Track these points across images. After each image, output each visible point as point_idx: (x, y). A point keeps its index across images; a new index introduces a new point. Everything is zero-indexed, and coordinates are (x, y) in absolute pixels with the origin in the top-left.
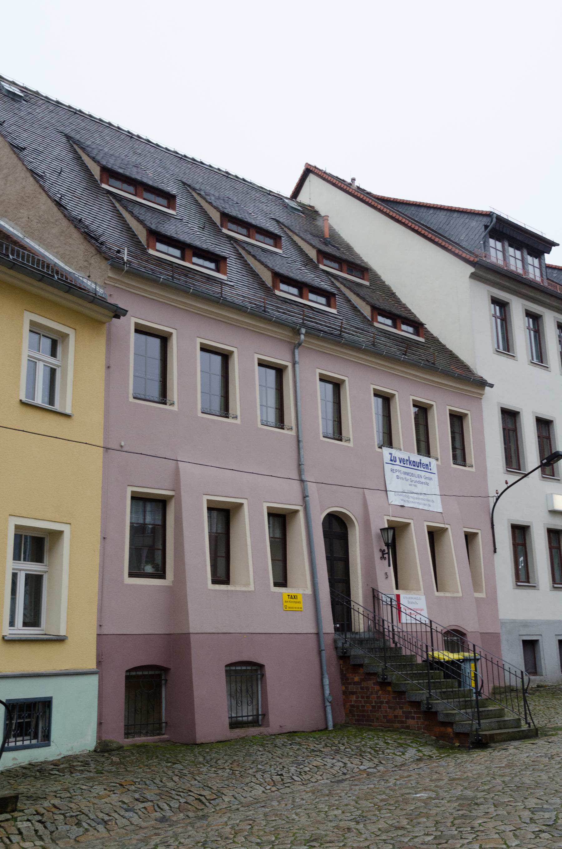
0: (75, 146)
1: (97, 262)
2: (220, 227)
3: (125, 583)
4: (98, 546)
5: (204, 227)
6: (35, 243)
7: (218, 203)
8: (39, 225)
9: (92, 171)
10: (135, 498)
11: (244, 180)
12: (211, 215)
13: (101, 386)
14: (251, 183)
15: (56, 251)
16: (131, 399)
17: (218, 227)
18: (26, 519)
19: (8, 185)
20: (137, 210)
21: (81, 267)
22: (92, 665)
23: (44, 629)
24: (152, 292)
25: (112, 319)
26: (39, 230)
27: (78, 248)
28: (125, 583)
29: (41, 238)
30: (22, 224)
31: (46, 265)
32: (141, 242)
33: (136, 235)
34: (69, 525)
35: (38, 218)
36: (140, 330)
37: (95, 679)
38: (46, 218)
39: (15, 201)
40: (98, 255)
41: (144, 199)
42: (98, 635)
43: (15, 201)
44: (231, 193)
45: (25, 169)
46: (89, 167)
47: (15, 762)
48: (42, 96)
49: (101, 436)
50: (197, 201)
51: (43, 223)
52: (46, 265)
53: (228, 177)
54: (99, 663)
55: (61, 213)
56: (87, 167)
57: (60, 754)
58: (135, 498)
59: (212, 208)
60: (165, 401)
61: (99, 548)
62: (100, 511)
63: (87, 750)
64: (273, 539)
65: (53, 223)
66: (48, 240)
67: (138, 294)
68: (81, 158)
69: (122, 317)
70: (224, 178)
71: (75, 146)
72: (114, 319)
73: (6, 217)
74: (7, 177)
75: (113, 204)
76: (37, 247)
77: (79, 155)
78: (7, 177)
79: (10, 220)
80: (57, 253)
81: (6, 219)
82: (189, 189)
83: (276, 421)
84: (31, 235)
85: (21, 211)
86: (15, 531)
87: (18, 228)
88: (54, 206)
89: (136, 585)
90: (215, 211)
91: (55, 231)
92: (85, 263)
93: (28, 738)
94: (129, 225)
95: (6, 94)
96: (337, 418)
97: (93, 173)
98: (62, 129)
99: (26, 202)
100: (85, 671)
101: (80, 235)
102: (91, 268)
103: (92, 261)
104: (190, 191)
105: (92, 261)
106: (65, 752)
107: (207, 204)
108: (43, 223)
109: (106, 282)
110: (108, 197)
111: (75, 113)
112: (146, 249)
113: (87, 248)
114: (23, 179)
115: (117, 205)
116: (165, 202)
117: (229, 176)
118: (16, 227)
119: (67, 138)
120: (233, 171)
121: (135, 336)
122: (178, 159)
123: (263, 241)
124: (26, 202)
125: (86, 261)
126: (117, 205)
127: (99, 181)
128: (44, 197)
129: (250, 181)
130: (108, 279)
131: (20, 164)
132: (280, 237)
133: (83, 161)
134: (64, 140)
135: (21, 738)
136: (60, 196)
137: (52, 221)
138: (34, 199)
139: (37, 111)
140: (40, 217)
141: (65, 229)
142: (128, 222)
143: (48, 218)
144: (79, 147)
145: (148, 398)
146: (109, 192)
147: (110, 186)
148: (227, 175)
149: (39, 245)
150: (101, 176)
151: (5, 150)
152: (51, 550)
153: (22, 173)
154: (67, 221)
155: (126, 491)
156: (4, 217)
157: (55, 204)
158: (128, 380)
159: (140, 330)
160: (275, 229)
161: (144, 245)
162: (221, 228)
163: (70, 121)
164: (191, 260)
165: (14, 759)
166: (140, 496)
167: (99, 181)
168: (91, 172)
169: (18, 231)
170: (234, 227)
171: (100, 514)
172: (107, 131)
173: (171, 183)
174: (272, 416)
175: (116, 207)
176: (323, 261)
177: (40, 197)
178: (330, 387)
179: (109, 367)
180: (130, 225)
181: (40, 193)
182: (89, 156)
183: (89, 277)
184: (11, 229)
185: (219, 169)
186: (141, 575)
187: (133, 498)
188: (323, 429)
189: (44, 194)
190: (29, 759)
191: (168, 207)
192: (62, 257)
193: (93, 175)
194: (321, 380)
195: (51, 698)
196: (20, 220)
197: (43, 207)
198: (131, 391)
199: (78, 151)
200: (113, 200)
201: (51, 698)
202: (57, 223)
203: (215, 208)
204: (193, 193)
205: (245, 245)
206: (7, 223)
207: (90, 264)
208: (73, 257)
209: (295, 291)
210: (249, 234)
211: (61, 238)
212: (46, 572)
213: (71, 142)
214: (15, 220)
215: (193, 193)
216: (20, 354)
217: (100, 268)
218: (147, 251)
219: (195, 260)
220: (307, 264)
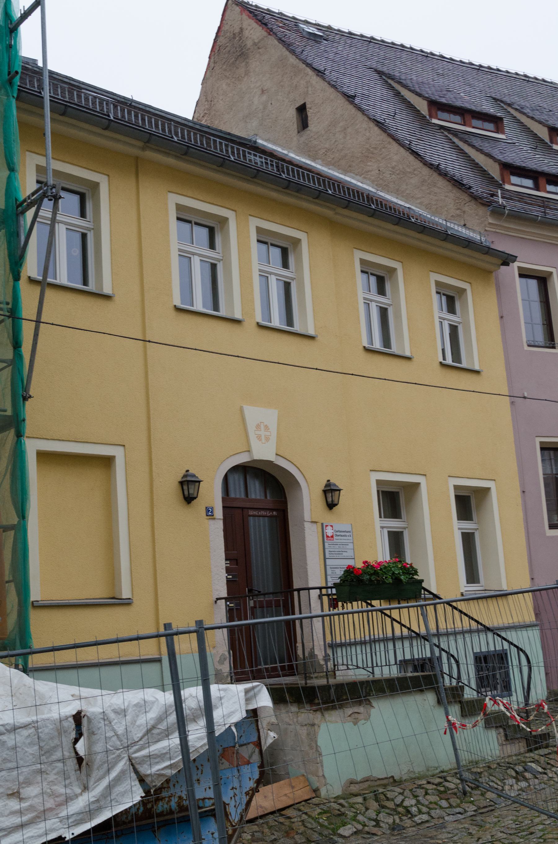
0: (390, 81)
1: (471, 208)
2: (549, 143)
5: (537, 147)
6: (392, 196)
7: (543, 117)
8: (393, 176)
9: (416, 106)
10: (545, 448)
11: (544, 80)
12: (535, 132)
13: (498, 337)
14: (551, 83)
15: (418, 201)
16: (526, 348)
17: (547, 143)
19: (348, 138)
20: (477, 142)
21: (452, 216)
23: (483, 585)
25: (499, 268)
26: (394, 182)
27: (446, 196)
29: (398, 190)
30: (373, 178)
32: (493, 178)
33: (485, 171)
34: (493, 482)
35: (390, 169)
36: (524, 274)
38: (401, 168)
39: (360, 155)
40: (473, 202)
41: (474, 127)
43: (360, 155)
44: (539, 100)
45: (366, 119)
46: (412, 103)
48: (335, 30)
49: (507, 388)
50: (515, 117)
51: (398, 174)
53: (528, 81)
54: (537, 615)
55: (419, 162)
56: (409, 102)
58: (545, 448)
59: (537, 124)
60: (553, 344)
61: (521, 502)
62: (516, 464)
64: (545, 476)
65: (410, 173)
66: (407, 192)
68: (400, 93)
69: (511, 264)
70: (525, 82)
71: (390, 81)
72: (502, 267)
73: (351, 172)
74: (345, 129)
75: (451, 139)
76: (395, 200)
77: (396, 90)
78: (345, 129)
79: (357, 175)
80: (421, 203)
81: (352, 174)
82: (502, 105)
83: (545, 340)
84: (386, 188)
85: (369, 164)
86: (455, 492)
87: (368, 182)
88: (410, 155)
90: (540, 126)
91: (414, 181)
92: (458, 212)
93: (488, 689)
94: (474, 161)
95: (308, 37)
96: (546, 320)
97: (418, 108)
98: (368, 63)
99: (373, 153)
101: (448, 183)
102: (465, 216)
103: (466, 209)
104: (505, 107)
105: (466, 209)
107: (529, 120)
108: (398, 174)
109: (487, 229)
110: (443, 133)
111: (370, 42)
112: (501, 185)
113: (458, 195)
114: (366, 130)
115: (455, 140)
116: (491, 126)
117: (530, 80)
118: (365, 181)
119: (379, 74)
120: (531, 74)
121: (520, 281)
122: (476, 71)
123: (481, 127)
124: (373, 153)
125: (458, 209)
126: (455, 140)
127: (428, 117)
128: (395, 146)
129: (550, 81)
130: (488, 226)
131: (359, 114)
132: (501, 119)
133: (402, 96)
134: (376, 76)
136: (409, 143)
137: (409, 170)
138: (383, 150)
139: (340, 49)
140: (393, 168)
141: (426, 178)
142: (472, 157)
143: (403, 168)
144: (395, 82)
145: (537, 344)
146: (442, 127)
147: (439, 120)
148: (527, 79)
149: (397, 198)
150: (429, 110)
151: (339, 101)
152: (478, 506)
153: (362, 123)
154: (428, 169)
155: (535, 442)
156: (348, 172)
157: (410, 153)
158: (521, 328)
159: (524, 274)
160: (489, 108)
161: (498, 180)
162: (551, 145)
163: (370, 52)
164: (510, 181)
166: (550, 446)
167: (428, 117)
168: (416, 108)
169: (369, 185)
170: (445, 115)
171: (516, 468)
172: (404, 55)
173: (485, 103)
174: (540, 336)
175: (454, 143)
176: (437, 115)
177: (389, 146)
178: (533, 284)
180: (477, 161)
181: (389, 143)
182: (410, 91)
183: (465, 225)
184: (359, 184)
185: (517, 74)
187: (542, 449)
188: (527, 337)
189: (394, 143)
191: (497, 132)
192: (428, 207)
193: (419, 111)
194: (521, 276)
196: (369, 173)
197: (396, 158)
198: (525, 340)
199: (395, 86)
200: (449, 136)
202: (415, 172)
203: (540, 122)
204: (509, 109)
205: (466, 137)
206: (353, 178)
207: (464, 212)
208: (441, 207)
209: (529, 183)
210: (464, 122)
211: (423, 188)
212: (476, 529)
213: (384, 77)
214: (363, 174)
215: (509, 109)
216: (433, 317)
217: (476, 215)
218: (503, 186)
219: (550, 188)
220: (537, 147)
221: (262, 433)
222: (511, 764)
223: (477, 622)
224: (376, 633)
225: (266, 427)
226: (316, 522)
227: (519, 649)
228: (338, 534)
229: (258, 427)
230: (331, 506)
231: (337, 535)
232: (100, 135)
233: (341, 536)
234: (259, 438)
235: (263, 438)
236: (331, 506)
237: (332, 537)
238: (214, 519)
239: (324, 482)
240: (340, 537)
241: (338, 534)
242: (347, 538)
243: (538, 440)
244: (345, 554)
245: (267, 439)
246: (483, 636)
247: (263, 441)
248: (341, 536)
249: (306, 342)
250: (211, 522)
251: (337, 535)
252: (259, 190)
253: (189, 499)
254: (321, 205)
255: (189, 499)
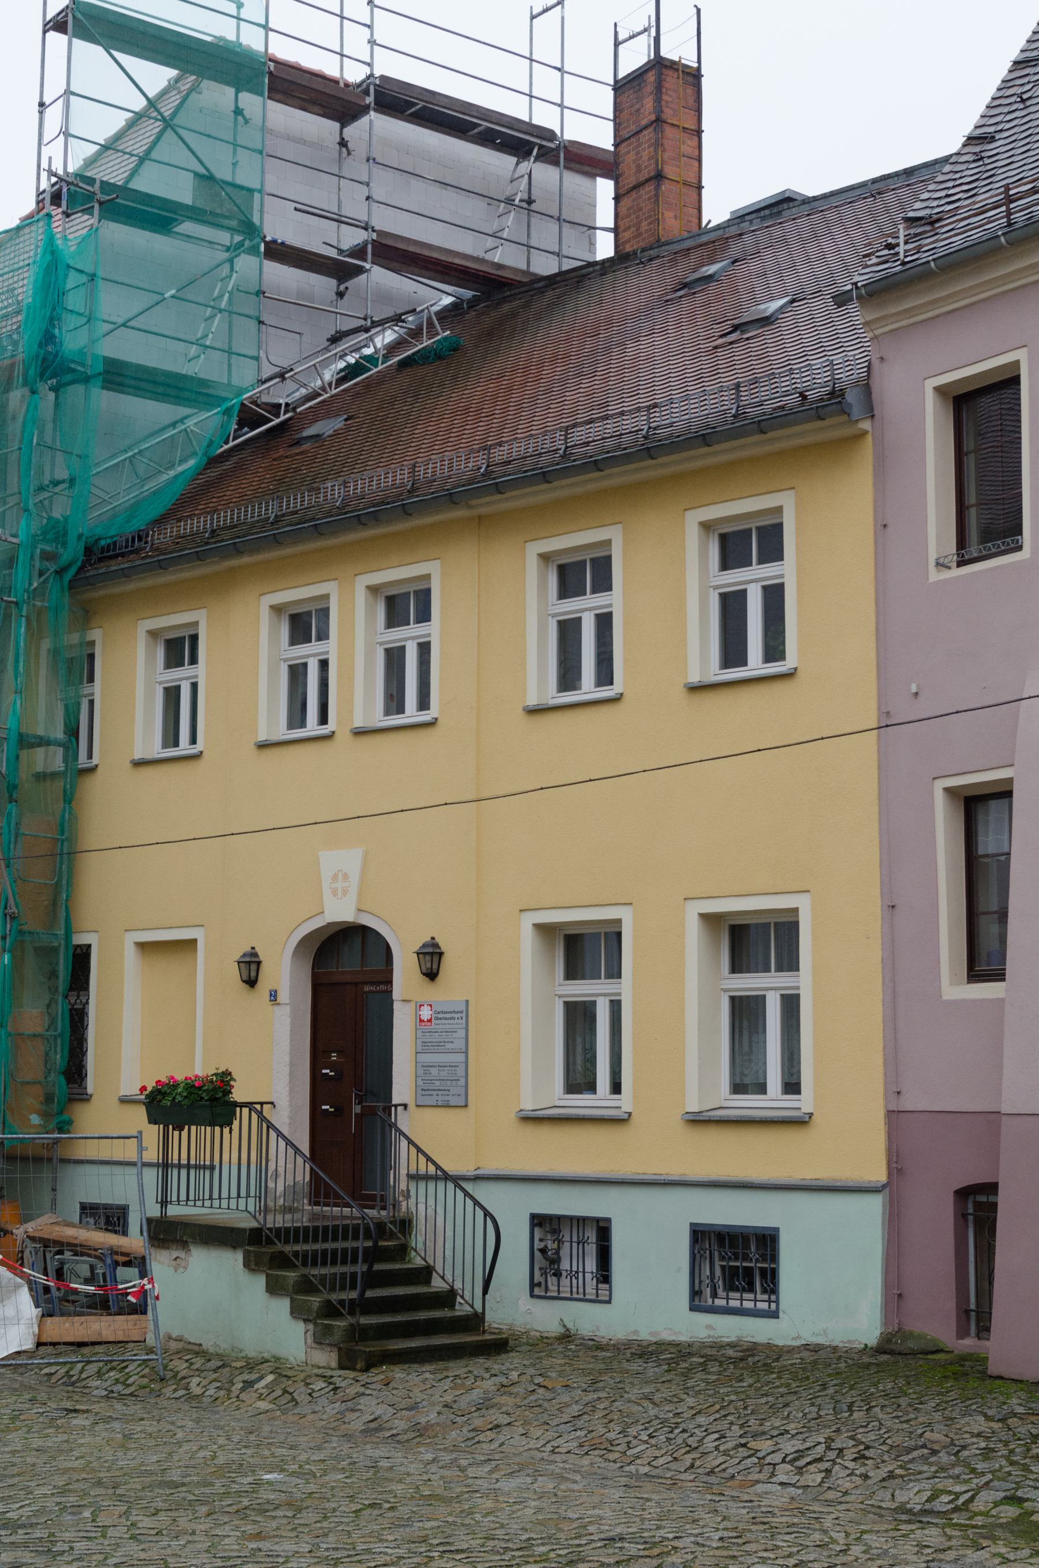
3: (945, 997)
4: (876, 927)
18: (718, 900)
22: (879, 1174)
24: (948, 296)
28: (945, 997)
31: (42, 579)
37: (875, 1205)
42: (890, 1113)
47: (711, 1333)
52: (42, 579)
57: (799, 1337)
63: (860, 1343)
67: (937, 316)
89: (964, 1001)
100: (851, 1184)
106: (809, 1336)
135: (737, 1295)
165: (709, 1327)
179: (885, 526)
186: (987, 975)
190: (739, 1333)
195: (777, 1230)
201: (777, 1230)
221: (339, 885)
222: (1032, 1487)
223: (429, 1159)
224: (184, 1155)
225: (346, 876)
226: (409, 1001)
227: (487, 1213)
228: (441, 1016)
229: (335, 877)
230: (432, 975)
231: (438, 1018)
232: (821, 429)
233: (446, 1019)
234: (334, 893)
235: (340, 892)
236: (432, 975)
237: (430, 1021)
238: (279, 1004)
239: (247, 949)
240: (444, 1021)
241: (441, 1016)
242: (456, 1021)
243: (940, 785)
244: (449, 1046)
245: (345, 892)
246: (441, 1185)
247: (340, 895)
248: (446, 1019)
249: (778, 687)
250: (276, 1008)
251: (438, 1018)
252: (288, 551)
253: (251, 982)
254: (663, 465)
255: (251, 982)
